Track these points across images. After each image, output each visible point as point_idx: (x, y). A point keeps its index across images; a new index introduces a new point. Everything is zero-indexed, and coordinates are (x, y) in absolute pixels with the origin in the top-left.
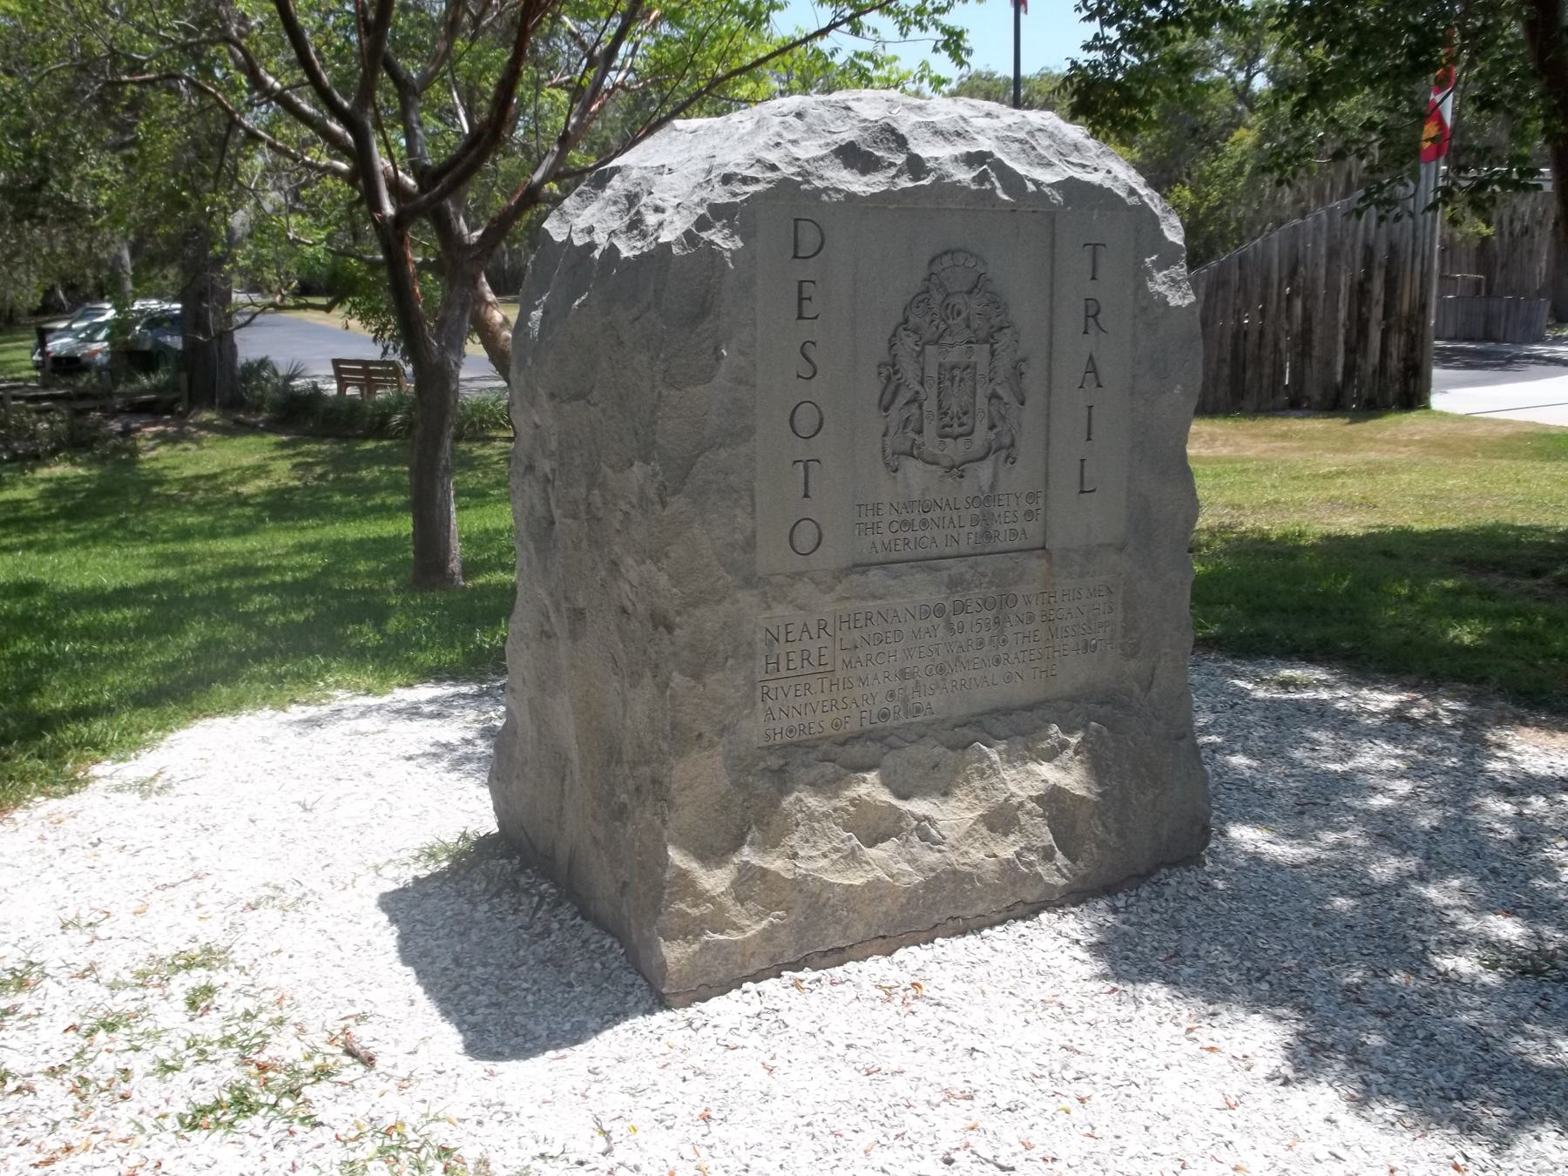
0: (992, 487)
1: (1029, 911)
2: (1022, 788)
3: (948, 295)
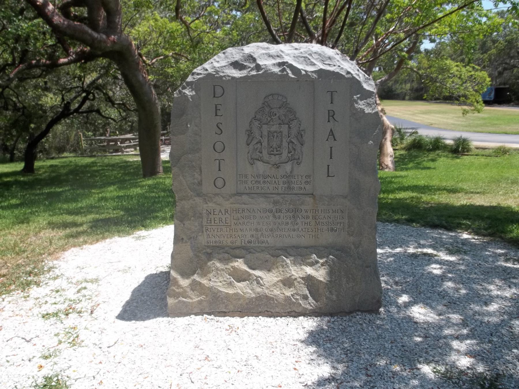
0: (291, 172)
1: (295, 315)
2: (297, 274)
3: (272, 109)
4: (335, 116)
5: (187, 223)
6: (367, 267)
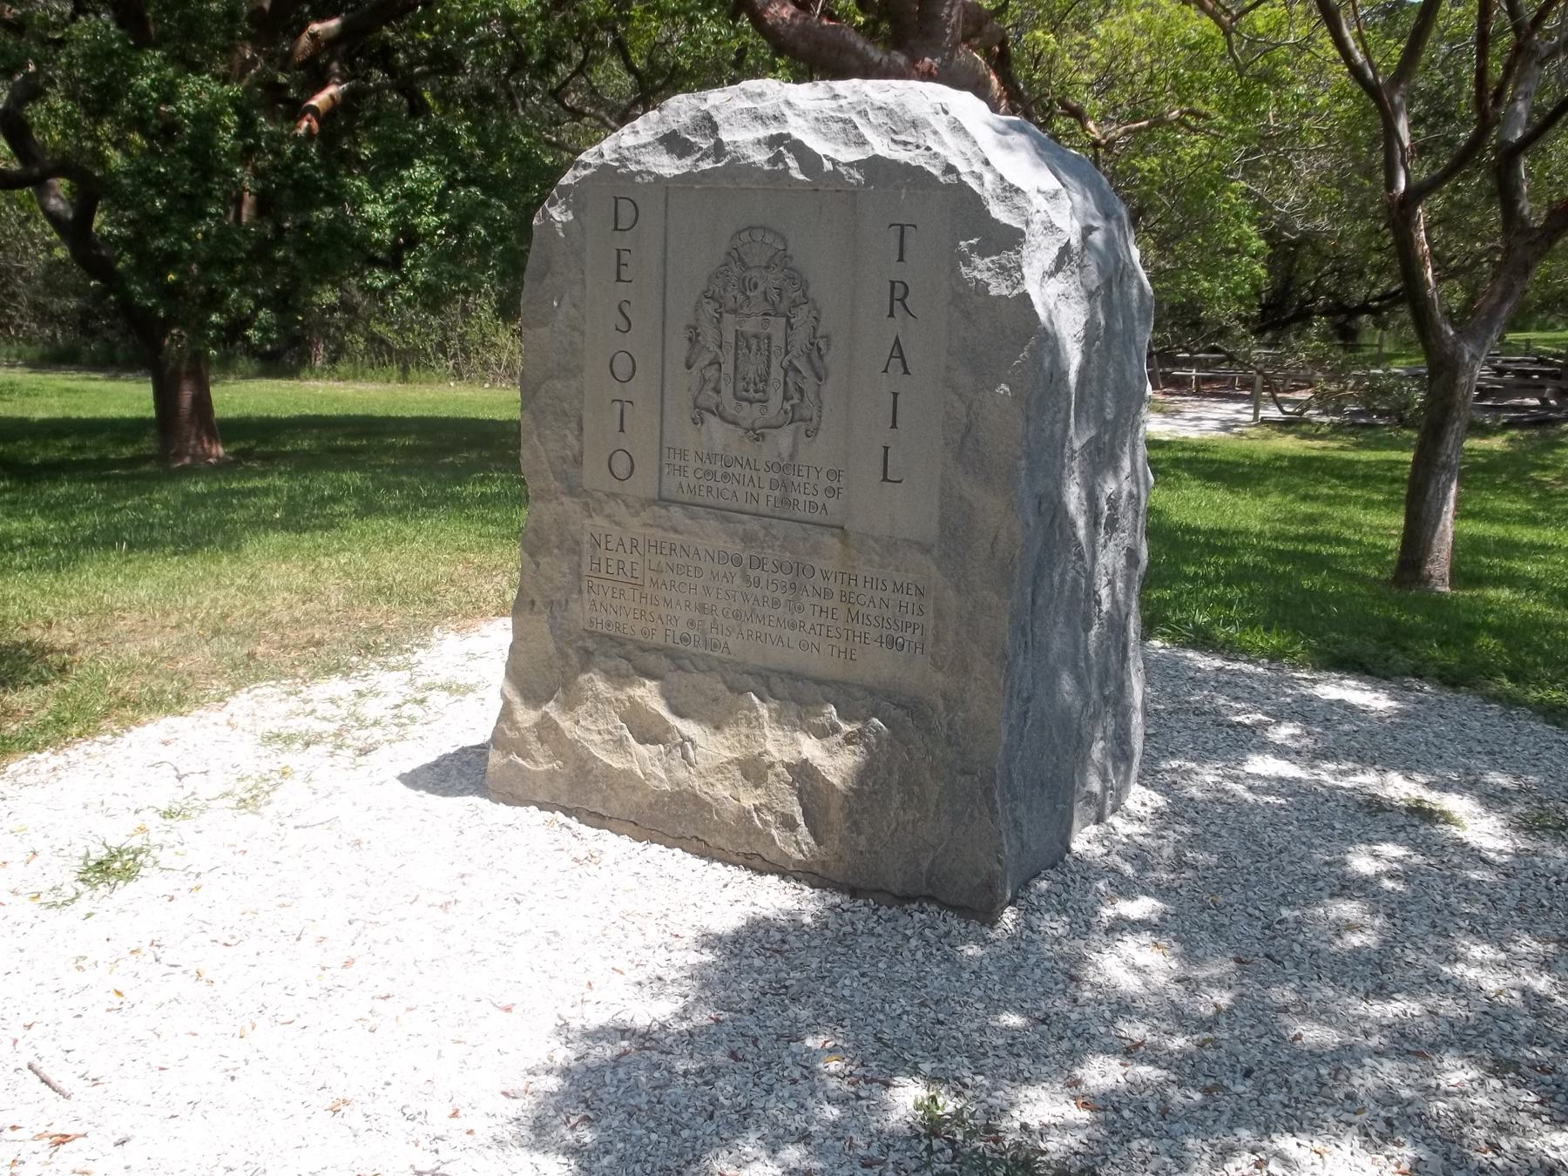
0: (792, 456)
3: (748, 268)
4: (907, 301)
5: (544, 561)
6: (964, 772)
